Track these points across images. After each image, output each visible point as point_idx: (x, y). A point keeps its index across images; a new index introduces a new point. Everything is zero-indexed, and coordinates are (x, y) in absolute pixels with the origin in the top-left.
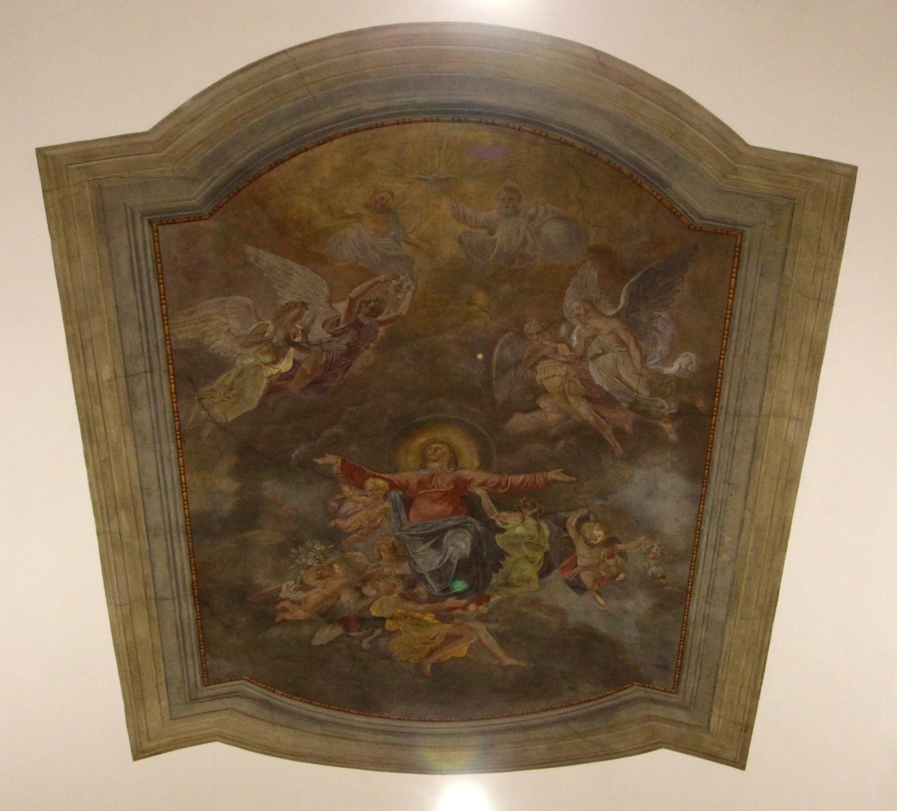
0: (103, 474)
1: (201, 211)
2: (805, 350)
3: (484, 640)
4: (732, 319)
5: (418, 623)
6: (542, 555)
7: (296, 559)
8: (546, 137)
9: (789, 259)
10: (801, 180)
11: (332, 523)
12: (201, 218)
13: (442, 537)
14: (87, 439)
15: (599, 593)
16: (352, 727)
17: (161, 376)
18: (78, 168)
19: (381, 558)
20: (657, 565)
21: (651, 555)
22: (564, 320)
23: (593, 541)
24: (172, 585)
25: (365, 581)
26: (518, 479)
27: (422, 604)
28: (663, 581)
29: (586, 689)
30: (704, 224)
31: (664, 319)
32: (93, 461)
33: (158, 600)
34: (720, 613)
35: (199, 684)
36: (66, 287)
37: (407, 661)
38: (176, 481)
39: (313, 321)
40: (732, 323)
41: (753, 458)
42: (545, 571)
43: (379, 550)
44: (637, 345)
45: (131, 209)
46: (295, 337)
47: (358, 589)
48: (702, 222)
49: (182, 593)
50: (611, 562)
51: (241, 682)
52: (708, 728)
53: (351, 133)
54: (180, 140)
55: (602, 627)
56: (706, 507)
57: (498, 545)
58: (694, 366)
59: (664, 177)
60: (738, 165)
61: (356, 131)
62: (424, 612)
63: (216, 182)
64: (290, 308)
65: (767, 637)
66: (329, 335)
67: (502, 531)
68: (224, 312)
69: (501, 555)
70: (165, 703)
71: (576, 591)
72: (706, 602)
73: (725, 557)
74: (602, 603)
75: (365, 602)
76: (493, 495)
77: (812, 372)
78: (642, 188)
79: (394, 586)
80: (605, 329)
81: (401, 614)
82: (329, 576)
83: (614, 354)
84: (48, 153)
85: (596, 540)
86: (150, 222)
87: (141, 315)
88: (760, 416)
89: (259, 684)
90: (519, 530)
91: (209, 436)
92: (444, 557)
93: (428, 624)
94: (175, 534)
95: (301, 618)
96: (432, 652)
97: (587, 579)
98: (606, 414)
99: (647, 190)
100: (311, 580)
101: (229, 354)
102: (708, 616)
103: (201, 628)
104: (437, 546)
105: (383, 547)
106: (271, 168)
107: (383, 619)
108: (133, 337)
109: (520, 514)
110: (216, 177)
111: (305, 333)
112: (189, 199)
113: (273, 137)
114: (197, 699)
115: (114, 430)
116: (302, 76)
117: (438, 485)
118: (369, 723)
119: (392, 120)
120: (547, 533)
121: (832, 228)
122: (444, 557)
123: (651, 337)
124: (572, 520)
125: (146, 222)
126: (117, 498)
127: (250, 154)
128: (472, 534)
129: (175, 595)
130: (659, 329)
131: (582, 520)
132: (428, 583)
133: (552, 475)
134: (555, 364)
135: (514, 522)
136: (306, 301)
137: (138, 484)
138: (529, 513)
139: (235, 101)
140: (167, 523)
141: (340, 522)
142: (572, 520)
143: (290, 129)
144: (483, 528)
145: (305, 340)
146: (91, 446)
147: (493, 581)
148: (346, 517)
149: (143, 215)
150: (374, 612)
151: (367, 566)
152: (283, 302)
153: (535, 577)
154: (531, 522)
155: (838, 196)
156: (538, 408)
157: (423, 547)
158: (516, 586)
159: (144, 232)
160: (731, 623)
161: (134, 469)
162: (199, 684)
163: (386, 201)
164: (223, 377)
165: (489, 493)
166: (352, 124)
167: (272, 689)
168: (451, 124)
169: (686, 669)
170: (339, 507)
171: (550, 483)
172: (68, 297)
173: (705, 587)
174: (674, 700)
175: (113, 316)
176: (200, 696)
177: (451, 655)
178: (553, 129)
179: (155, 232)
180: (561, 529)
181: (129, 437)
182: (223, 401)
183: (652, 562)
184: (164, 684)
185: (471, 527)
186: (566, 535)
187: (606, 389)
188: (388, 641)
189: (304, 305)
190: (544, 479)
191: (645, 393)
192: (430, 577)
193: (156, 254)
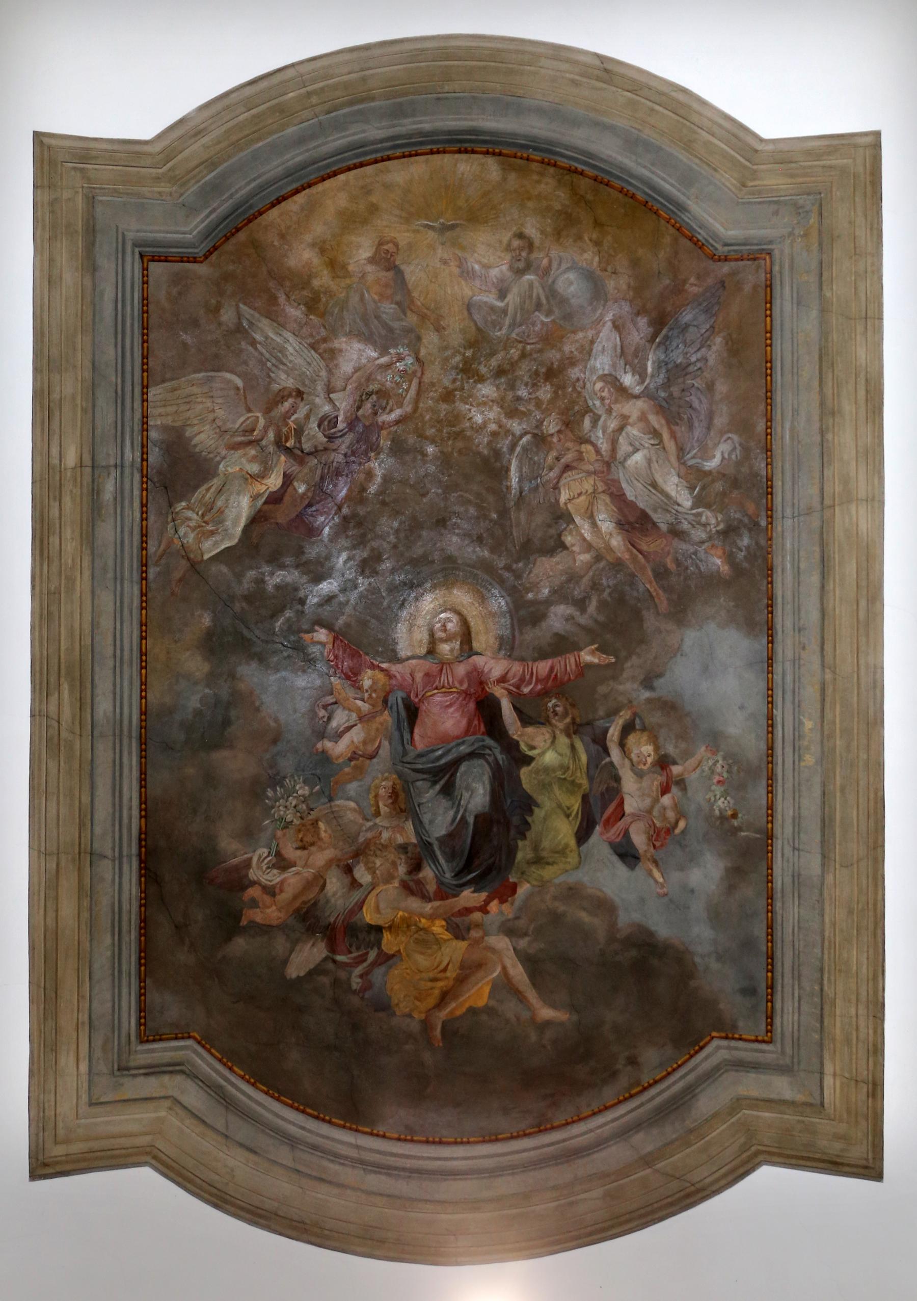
0: (49, 613)
1: (196, 251)
2: (862, 393)
3: (512, 972)
4: (774, 376)
5: (426, 941)
6: (580, 800)
7: (273, 807)
8: (555, 165)
9: (826, 275)
10: (824, 167)
11: (319, 746)
12: (195, 260)
13: (453, 775)
14: (38, 552)
15: (656, 862)
16: (336, 1157)
17: (132, 474)
18: (75, 168)
19: (377, 813)
20: (725, 794)
21: (716, 778)
22: (588, 410)
23: (641, 767)
24: (114, 832)
25: (357, 855)
26: (543, 667)
27: (430, 900)
28: (735, 823)
29: (651, 1056)
30: (729, 251)
31: (698, 389)
32: (41, 590)
33: (94, 856)
34: (812, 864)
35: (133, 1038)
36: (42, 320)
37: (410, 1016)
38: (135, 648)
39: (307, 417)
40: (774, 380)
41: (823, 577)
42: (583, 835)
43: (376, 796)
44: (673, 435)
45: (123, 234)
46: (287, 441)
47: (349, 870)
48: (726, 248)
49: (125, 853)
50: (666, 800)
51: (189, 1042)
52: (822, 1104)
53: (355, 167)
54: (180, 157)
55: (663, 930)
56: (775, 677)
57: (524, 786)
58: (738, 452)
59: (682, 198)
60: (755, 167)
61: (361, 165)
62: (432, 917)
63: (213, 216)
64: (283, 397)
65: (880, 893)
66: (326, 440)
67: (528, 760)
68: (211, 394)
69: (528, 804)
70: (84, 1067)
71: (624, 862)
72: (794, 848)
73: (809, 759)
74: (661, 880)
75: (357, 896)
76: (516, 698)
77: (874, 424)
78: (659, 216)
79: (394, 864)
80: (635, 415)
81: (403, 919)
82: (312, 844)
83: (645, 451)
84: (46, 140)
85: (645, 764)
86: (142, 256)
87: (119, 381)
88: (822, 510)
89: (213, 1051)
90: (550, 758)
91: (180, 580)
92: (457, 812)
93: (438, 942)
94: (126, 741)
95: (275, 923)
96: (445, 997)
97: (639, 840)
98: (644, 548)
99: (664, 218)
100: (290, 852)
101: (211, 456)
102: (799, 875)
103: (144, 924)
104: (448, 791)
105: (382, 792)
106: (273, 205)
107: (379, 929)
108: (106, 414)
109: (549, 729)
110: (214, 210)
111: (299, 432)
112: (184, 233)
113: (274, 167)
114: (128, 1069)
115: (70, 546)
116: (309, 94)
117: (448, 683)
118: (358, 1147)
119: (398, 152)
120: (584, 758)
121: (866, 216)
122: (457, 812)
123: (685, 417)
124: (614, 733)
125: (137, 256)
126: (62, 660)
127: (253, 185)
128: (491, 768)
129: (117, 854)
130: (694, 405)
131: (628, 729)
132: (436, 856)
133: (588, 657)
134: (580, 475)
135: (542, 744)
136: (302, 389)
137: (89, 642)
138: (561, 725)
139: (241, 118)
140: (118, 716)
141: (328, 744)
142: (614, 733)
143: (296, 157)
144: (504, 757)
145: (298, 445)
146: (41, 565)
147: (520, 856)
148: (339, 735)
149: (135, 245)
150: (369, 916)
151: (362, 825)
152: (276, 387)
153: (573, 842)
154: (563, 740)
155: (865, 173)
156: (564, 547)
157: (431, 793)
158: (548, 864)
159: (133, 267)
160: (829, 878)
161: (88, 617)
162: (133, 1038)
163: (392, 255)
164: (202, 489)
165: (510, 692)
166: (357, 156)
167: (229, 1064)
168: (457, 156)
169: (780, 981)
170: (329, 719)
171: (583, 669)
172: (42, 334)
173: (789, 821)
174: (770, 1058)
175: (88, 374)
176: (132, 1064)
177: (467, 1005)
178: (563, 156)
179: (145, 269)
180: (600, 749)
181: (86, 563)
182: (200, 526)
183: (718, 790)
184: (87, 1027)
185: (489, 755)
186: (608, 760)
187: (641, 505)
188: (386, 974)
189: (300, 394)
190: (577, 665)
191: (686, 501)
192: (440, 848)
193: (143, 300)
